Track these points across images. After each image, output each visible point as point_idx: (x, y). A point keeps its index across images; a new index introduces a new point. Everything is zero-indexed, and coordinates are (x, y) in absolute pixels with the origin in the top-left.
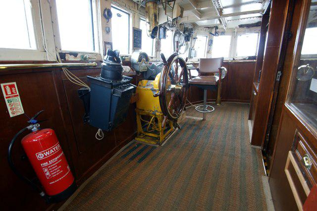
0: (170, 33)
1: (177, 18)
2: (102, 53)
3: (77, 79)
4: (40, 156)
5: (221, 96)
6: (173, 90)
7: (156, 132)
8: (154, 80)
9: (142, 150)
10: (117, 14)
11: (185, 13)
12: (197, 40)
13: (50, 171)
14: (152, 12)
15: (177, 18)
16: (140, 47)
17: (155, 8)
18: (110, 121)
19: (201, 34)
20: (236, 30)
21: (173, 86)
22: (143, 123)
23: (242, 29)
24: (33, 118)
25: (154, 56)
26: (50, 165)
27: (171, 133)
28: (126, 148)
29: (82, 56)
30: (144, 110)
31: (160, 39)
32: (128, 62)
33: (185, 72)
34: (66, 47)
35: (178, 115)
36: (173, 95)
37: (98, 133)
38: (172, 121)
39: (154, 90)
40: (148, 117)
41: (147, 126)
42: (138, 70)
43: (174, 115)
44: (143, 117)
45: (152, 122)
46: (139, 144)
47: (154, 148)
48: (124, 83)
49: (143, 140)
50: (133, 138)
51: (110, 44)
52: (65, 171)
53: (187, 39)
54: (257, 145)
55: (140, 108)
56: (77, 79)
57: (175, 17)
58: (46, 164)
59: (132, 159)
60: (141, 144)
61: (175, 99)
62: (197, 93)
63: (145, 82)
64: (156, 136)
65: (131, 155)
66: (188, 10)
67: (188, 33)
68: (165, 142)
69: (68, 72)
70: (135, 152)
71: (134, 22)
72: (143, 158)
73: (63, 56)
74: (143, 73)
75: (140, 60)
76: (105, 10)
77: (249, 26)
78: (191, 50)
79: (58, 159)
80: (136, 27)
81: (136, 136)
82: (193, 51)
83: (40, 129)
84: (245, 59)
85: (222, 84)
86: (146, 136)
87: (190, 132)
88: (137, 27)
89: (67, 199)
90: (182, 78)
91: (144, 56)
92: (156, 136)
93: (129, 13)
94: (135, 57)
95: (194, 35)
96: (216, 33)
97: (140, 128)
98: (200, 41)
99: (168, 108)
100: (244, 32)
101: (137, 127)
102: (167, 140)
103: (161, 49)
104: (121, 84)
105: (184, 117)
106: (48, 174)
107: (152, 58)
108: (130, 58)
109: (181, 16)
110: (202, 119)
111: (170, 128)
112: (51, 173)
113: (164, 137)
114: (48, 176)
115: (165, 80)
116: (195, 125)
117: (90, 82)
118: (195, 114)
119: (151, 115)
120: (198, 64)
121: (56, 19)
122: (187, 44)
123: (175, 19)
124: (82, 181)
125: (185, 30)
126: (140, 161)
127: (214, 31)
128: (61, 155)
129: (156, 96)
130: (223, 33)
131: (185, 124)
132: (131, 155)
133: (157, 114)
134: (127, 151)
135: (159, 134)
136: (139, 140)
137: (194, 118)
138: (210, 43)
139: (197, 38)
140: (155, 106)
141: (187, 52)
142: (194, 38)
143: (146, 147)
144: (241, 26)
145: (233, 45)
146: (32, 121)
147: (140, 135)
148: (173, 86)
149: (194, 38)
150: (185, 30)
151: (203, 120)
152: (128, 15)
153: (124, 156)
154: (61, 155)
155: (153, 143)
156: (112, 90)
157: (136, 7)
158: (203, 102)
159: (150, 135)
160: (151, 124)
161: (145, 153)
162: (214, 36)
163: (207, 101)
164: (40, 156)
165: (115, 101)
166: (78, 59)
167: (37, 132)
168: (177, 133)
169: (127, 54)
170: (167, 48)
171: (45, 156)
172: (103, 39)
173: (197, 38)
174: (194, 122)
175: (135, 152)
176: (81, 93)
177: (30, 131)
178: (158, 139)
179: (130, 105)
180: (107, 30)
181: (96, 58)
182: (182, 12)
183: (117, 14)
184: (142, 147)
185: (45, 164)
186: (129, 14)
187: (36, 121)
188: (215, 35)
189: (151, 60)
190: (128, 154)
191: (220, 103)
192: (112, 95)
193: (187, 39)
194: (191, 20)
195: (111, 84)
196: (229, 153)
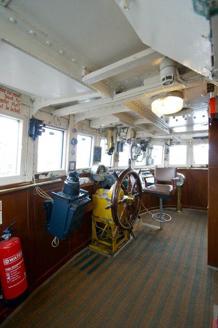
0: (127, 147)
2: (67, 170)
3: (44, 193)
4: (6, 262)
5: (182, 202)
6: (126, 201)
7: (110, 241)
8: (109, 189)
9: (93, 261)
13: (11, 276)
14: (110, 135)
18: (65, 231)
20: (190, 141)
21: (126, 197)
22: (97, 230)
23: (195, 140)
24: (7, 229)
25: (112, 165)
26: (12, 270)
27: (125, 242)
29: (51, 175)
30: (98, 217)
32: (88, 173)
33: (138, 183)
34: (40, 169)
35: (131, 225)
36: (125, 206)
37: (54, 240)
38: (124, 229)
39: (107, 199)
40: (101, 225)
41: (102, 232)
42: (96, 180)
43: (127, 225)
44: (98, 224)
45: (106, 229)
46: (92, 253)
47: (106, 258)
48: (81, 197)
49: (96, 248)
50: (87, 245)
51: (75, 162)
52: (22, 277)
54: (214, 266)
55: (96, 215)
56: (44, 193)
58: (9, 269)
59: (83, 269)
60: (94, 252)
61: (128, 208)
62: (149, 201)
63: (101, 190)
64: (109, 245)
65: (83, 264)
67: (145, 145)
68: (118, 253)
69: (40, 190)
70: (86, 262)
71: (95, 143)
72: (93, 269)
73: (37, 176)
74: (101, 182)
75: (98, 172)
76: (73, 139)
77: (202, 138)
78: (148, 157)
79: (19, 266)
80: (97, 145)
81: (90, 242)
82: (150, 160)
83: (10, 238)
84: (203, 167)
85: (181, 191)
86: (100, 243)
87: (146, 242)
89: (19, 304)
90: (136, 186)
91: (102, 169)
92: (109, 245)
94: (94, 169)
95: (150, 145)
96: (171, 144)
97: (94, 235)
98: (204, 116)
99: (120, 219)
100: (199, 143)
101: (92, 232)
102: (119, 251)
104: (77, 199)
105: (139, 224)
106: (9, 278)
107: (110, 168)
108: (90, 170)
110: (159, 228)
111: (123, 237)
112: (11, 278)
113: (118, 245)
114: (8, 280)
115: (117, 192)
116: (150, 235)
117: (53, 196)
118: (150, 222)
119: (105, 223)
120: (154, 170)
121: (37, 152)
124: (35, 288)
125: (142, 142)
126: (90, 272)
127: (168, 143)
128: (21, 262)
129: (108, 208)
130: (178, 143)
131: (141, 232)
132: (83, 264)
133: (111, 222)
134: (80, 258)
135: (112, 243)
136: (93, 247)
137: (152, 226)
138: (167, 151)
140: (107, 215)
141: (145, 161)
143: (99, 255)
144: (195, 138)
145: (190, 154)
146: (6, 231)
147: (94, 242)
148: (126, 197)
150: (142, 142)
151: (161, 229)
152: (90, 138)
153: (76, 265)
154: (21, 262)
155: (105, 252)
156: (70, 205)
158: (159, 208)
159: (104, 243)
160: (105, 231)
161: (96, 263)
163: (163, 207)
164: (6, 262)
165: (71, 213)
166: (48, 177)
167: (8, 240)
168: (131, 243)
169: (88, 167)
170: (123, 164)
171: (10, 262)
172: (69, 159)
174: (151, 231)
175: (86, 262)
176: (45, 204)
177: (3, 239)
178: (110, 248)
179: (86, 214)
180: (73, 153)
181: (61, 174)
184: (94, 256)
185: (8, 269)
186: (63, 132)
187: (9, 232)
189: (109, 169)
190: (80, 262)
191: (181, 210)
192: (69, 209)
193: (144, 149)
195: (69, 200)
196: (183, 273)
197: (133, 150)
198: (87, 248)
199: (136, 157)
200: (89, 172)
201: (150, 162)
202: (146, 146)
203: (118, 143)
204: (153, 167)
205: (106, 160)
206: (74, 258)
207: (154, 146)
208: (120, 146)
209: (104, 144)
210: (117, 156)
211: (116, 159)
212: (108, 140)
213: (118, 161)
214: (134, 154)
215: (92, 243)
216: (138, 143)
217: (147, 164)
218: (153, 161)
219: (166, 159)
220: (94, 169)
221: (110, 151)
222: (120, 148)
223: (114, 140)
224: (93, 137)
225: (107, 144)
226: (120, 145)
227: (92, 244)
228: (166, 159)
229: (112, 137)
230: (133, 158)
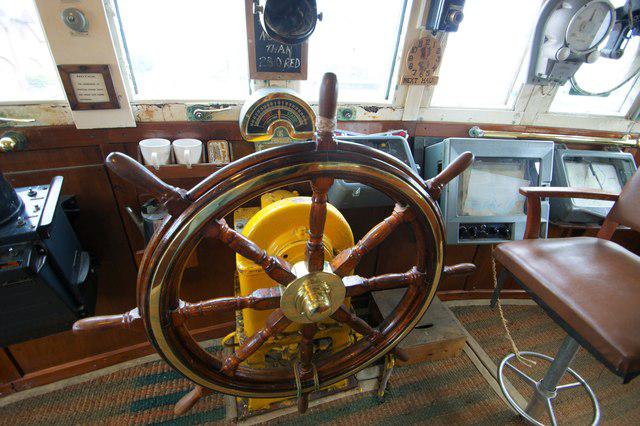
107: (374, 109)
230: (542, 69)
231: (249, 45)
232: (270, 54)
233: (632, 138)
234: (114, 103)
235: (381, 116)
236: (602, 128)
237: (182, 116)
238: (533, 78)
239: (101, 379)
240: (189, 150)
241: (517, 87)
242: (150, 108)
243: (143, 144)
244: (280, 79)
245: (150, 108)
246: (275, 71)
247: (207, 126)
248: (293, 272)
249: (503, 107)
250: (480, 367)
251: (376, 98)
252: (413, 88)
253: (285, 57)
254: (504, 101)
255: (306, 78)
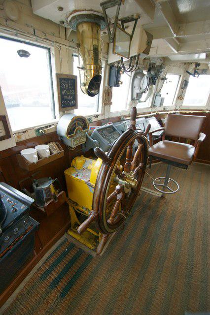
0: (126, 78)
1: (139, 55)
10: (19, 52)
11: (155, 42)
12: (165, 81)
14: (89, 44)
15: (139, 55)
16: (75, 106)
17: (95, 37)
19: (171, 73)
23: (16, 103)
25: (100, 112)
28: (56, 250)
31: (111, 87)
53: (152, 81)
57: (134, 53)
59: (54, 284)
66: (160, 38)
67: (155, 72)
71: (59, 64)
75: (71, 131)
80: (66, 72)
82: (158, 99)
88: (67, 73)
91: (80, 123)
93: (48, 47)
94: (63, 124)
95: (162, 75)
103: (112, 101)
107: (97, 116)
108: (56, 127)
109: (147, 52)
122: (151, 89)
123: (135, 56)
138: (184, 84)
139: (166, 79)
141: (150, 100)
142: (162, 79)
145: (199, 57)
149: (162, 79)
151: (162, 197)
152: (45, 51)
157: (62, 34)
162: (191, 77)
173: (166, 79)
182: (149, 43)
183: (19, 52)
184: (73, 253)
186: (49, 50)
188: (194, 75)
193: (152, 81)
194: (162, 53)
197: (136, 82)
198: (65, 236)
199: (139, 95)
200: (53, 131)
201: (157, 103)
202: (157, 75)
203: (111, 66)
204: (158, 109)
205: (87, 106)
206: (44, 258)
207: (168, 76)
208: (115, 72)
209: (80, 73)
210: (108, 95)
211: (107, 100)
212: (84, 60)
213: (111, 103)
214: (137, 91)
215: (72, 228)
216: (145, 69)
217: (153, 106)
218: (162, 100)
219: (180, 97)
220: (63, 124)
221: (93, 87)
222: (113, 80)
223: (101, 56)
224: (53, 49)
225: (83, 68)
226: (114, 71)
227: (71, 230)
228: (180, 97)
229: (96, 51)
230: (135, 96)
231: (59, 97)
232: (66, 100)
233: (153, 113)
234: (8, 135)
235: (99, 118)
236: (198, 109)
237: (33, 135)
238: (133, 99)
239: (20, 294)
240: (45, 149)
241: (129, 102)
242: (20, 134)
243: (22, 152)
244: (69, 110)
245: (20, 134)
246: (180, 164)
247: (47, 136)
248: (74, 75)
249: (171, 105)
250: (145, 191)
251: (95, 113)
252: (106, 106)
253: (70, 100)
254: (53, 117)
255: (77, 108)
